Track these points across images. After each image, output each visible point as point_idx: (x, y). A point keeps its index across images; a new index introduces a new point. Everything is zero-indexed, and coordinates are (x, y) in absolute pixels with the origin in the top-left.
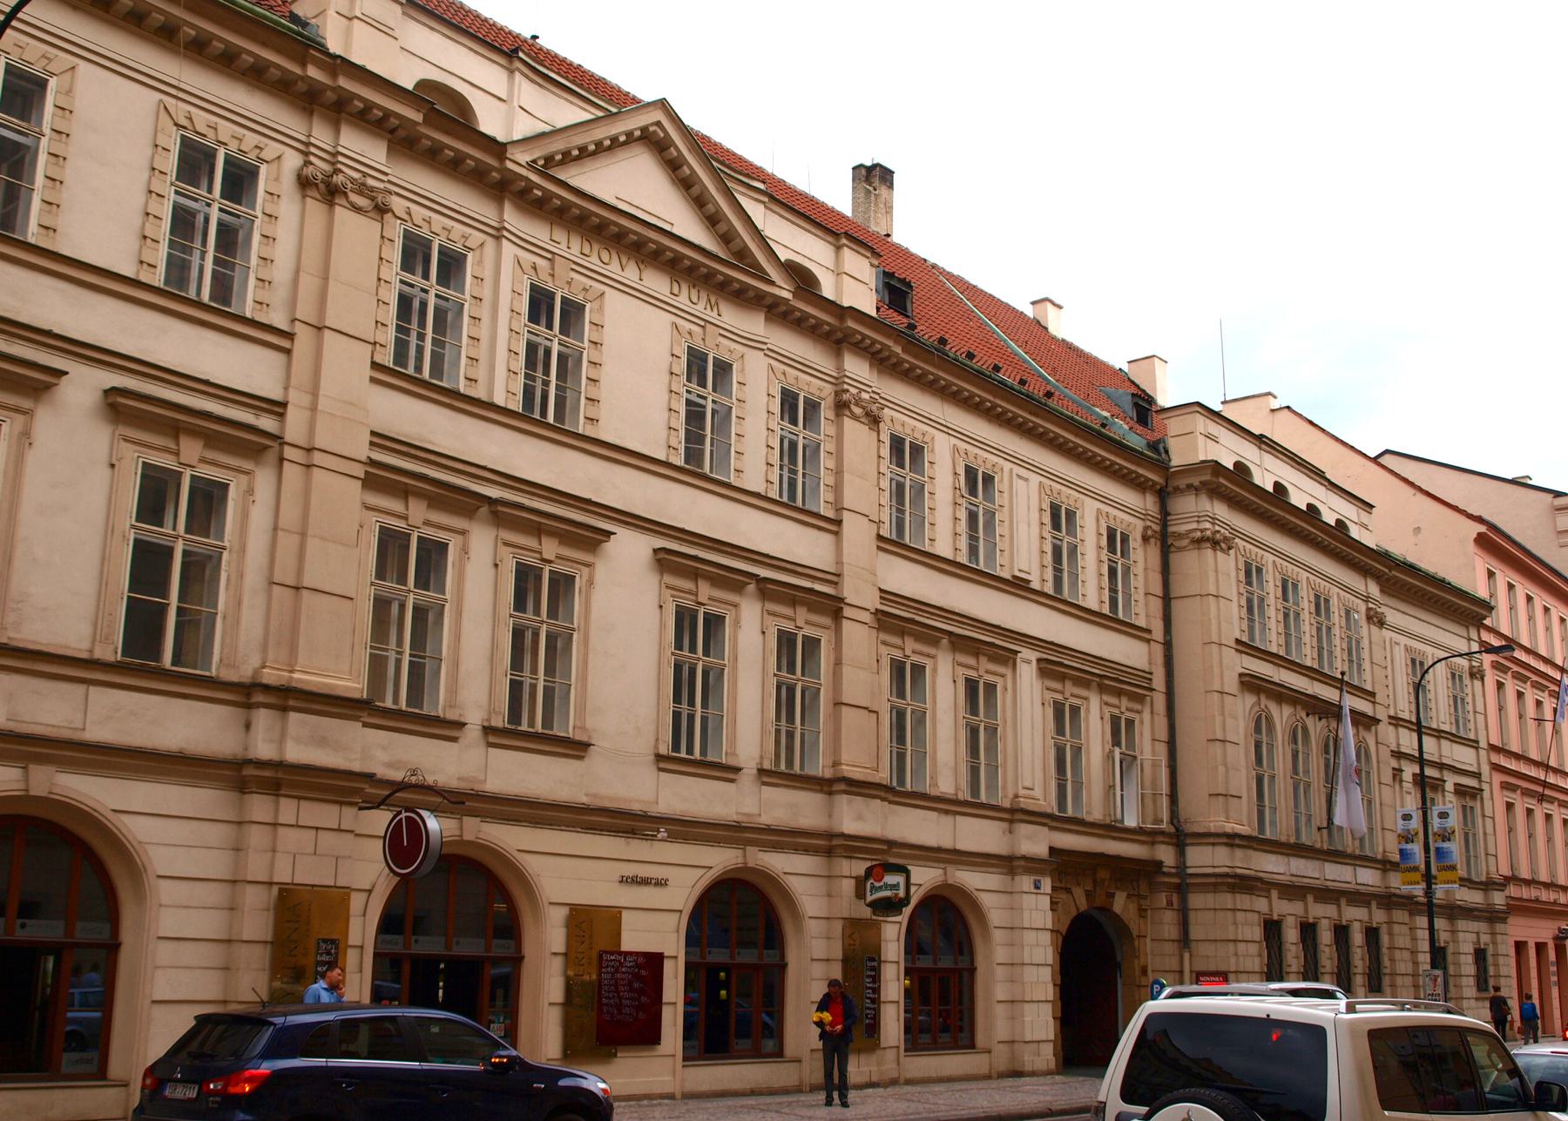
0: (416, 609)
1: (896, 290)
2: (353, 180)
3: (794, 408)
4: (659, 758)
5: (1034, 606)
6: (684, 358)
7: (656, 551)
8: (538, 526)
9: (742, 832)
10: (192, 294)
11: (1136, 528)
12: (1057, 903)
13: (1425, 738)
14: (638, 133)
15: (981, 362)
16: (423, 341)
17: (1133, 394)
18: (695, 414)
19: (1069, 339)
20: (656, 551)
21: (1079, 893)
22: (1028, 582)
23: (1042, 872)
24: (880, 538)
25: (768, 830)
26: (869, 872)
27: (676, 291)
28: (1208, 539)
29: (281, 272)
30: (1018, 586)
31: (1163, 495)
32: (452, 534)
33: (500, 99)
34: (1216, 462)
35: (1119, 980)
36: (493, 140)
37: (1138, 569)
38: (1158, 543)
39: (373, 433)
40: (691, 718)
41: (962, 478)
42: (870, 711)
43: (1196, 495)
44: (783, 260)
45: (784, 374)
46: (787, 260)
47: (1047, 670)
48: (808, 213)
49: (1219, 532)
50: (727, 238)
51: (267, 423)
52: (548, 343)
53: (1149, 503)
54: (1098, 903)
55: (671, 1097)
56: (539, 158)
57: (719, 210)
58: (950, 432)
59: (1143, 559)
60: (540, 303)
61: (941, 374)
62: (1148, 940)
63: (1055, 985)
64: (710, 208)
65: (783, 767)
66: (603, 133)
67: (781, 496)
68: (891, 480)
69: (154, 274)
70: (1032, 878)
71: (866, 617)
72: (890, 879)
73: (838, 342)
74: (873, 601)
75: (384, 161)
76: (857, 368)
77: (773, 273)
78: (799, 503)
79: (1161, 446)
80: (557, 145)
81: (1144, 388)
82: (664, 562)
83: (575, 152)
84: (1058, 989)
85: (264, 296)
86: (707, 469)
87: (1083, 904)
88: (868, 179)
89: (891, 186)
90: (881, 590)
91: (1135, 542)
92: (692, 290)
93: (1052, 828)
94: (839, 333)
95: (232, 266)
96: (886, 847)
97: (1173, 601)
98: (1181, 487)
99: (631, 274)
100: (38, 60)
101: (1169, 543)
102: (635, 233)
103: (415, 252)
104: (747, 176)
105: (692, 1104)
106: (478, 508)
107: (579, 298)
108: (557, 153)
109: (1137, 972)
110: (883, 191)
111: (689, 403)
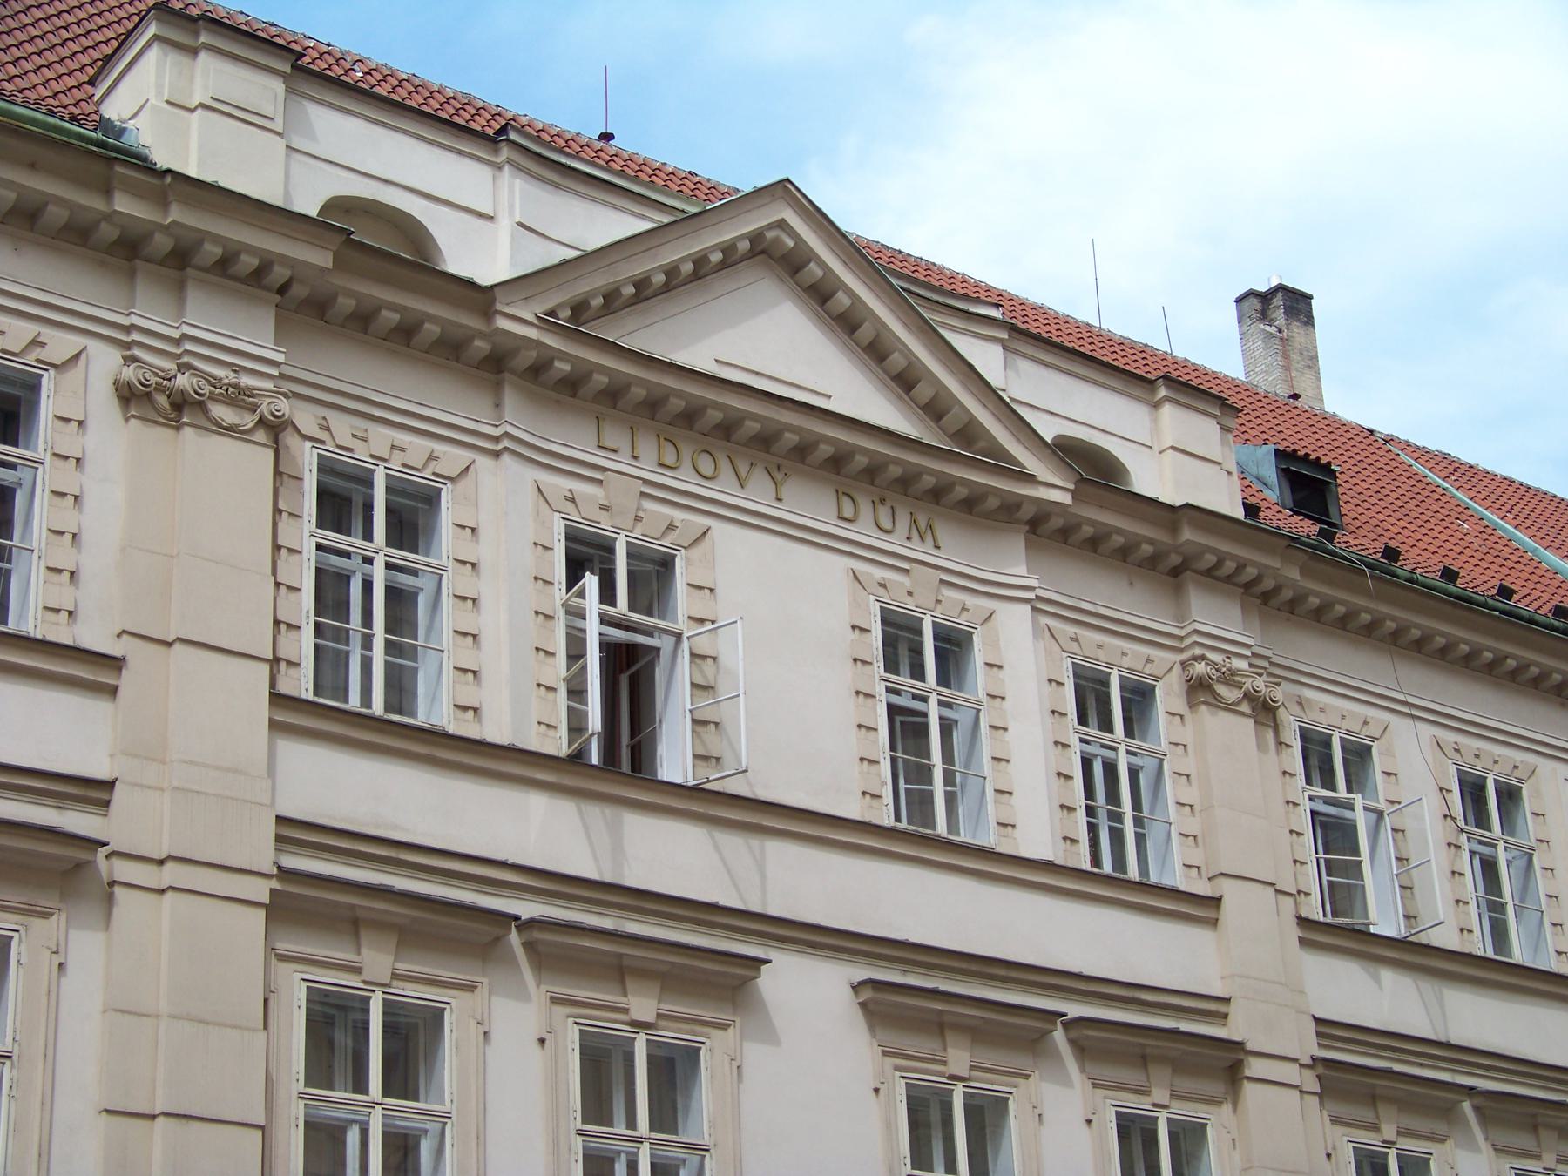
0: (388, 1136)
2: (215, 382)
3: (1328, 760)
7: (856, 988)
10: (354, 702)
15: (1527, 600)
20: (856, 988)
24: (1303, 922)
27: (848, 511)
29: (96, 560)
33: (481, 215)
36: (469, 284)
39: (280, 820)
41: (1456, 797)
44: (1049, 439)
45: (1076, 640)
46: (1057, 437)
50: (936, 410)
52: (1109, 754)
56: (560, 305)
57: (913, 362)
58: (1415, 712)
61: (1385, 609)
64: (897, 361)
66: (678, 252)
68: (1472, 853)
74: (1308, 1045)
75: (1022, 570)
78: (1133, 873)
80: (592, 284)
85: (468, 696)
86: (941, 828)
88: (1264, 316)
89: (1309, 321)
90: (1317, 1020)
95: (411, 653)
99: (758, 495)
100: (1362, 729)
104: (965, 297)
106: (497, 939)
110: (1297, 331)
111: (893, 710)
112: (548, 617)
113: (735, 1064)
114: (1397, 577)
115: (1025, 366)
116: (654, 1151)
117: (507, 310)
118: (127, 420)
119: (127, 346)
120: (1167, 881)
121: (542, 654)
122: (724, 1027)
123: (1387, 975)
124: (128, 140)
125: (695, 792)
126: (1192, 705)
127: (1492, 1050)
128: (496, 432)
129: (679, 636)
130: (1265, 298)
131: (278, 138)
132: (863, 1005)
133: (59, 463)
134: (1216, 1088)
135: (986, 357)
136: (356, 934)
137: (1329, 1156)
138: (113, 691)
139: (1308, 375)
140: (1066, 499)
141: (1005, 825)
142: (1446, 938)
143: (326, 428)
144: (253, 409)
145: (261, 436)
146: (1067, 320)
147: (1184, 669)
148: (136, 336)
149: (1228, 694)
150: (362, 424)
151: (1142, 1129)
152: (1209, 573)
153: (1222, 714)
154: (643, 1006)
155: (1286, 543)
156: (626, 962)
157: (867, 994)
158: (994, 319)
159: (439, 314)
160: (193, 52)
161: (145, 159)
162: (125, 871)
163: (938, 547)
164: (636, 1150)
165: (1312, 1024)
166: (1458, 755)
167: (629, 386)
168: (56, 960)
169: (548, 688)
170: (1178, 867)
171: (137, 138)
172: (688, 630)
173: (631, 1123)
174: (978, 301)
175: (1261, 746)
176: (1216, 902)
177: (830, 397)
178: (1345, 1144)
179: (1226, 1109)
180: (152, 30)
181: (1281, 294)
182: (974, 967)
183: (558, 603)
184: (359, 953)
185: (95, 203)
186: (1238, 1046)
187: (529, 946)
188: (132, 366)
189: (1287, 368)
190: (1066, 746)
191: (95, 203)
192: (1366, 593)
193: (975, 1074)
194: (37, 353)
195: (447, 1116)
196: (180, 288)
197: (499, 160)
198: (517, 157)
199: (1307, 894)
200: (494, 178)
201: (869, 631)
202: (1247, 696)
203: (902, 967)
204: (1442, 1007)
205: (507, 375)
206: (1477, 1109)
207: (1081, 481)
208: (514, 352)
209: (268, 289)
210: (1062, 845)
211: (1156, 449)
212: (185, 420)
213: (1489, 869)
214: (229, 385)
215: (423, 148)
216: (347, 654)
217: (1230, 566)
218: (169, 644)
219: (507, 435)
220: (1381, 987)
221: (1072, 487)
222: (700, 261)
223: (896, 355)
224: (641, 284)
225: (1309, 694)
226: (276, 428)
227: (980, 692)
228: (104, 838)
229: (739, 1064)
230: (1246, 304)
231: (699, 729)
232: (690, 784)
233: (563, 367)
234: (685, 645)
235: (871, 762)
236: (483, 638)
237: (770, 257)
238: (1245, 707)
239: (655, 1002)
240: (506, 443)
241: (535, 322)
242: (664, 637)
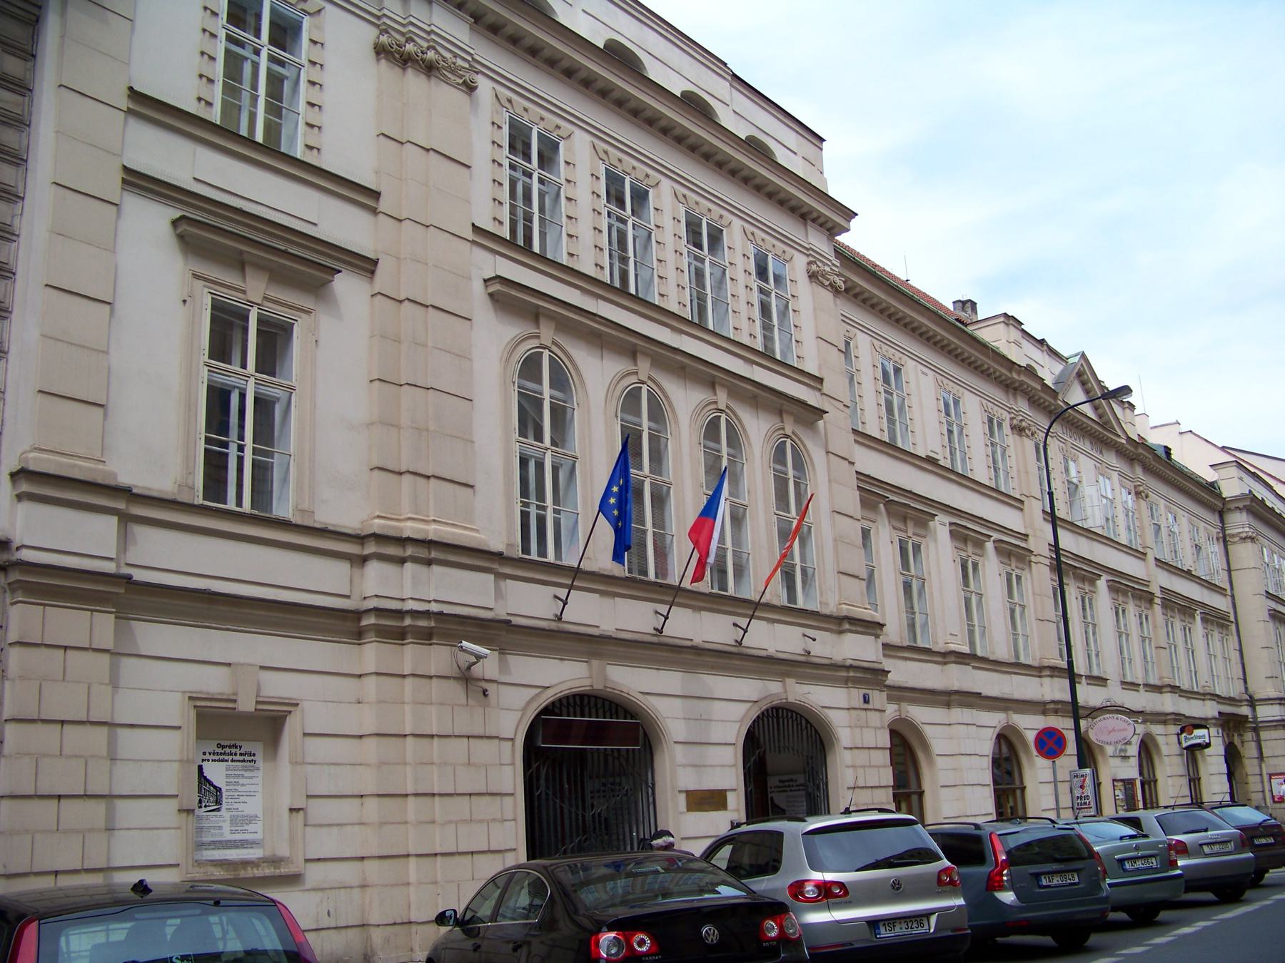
0: (257, 400)
4: (1123, 683)
5: (1111, 549)
7: (175, 223)
9: (836, 671)
13: (1060, 531)
20: (175, 223)
25: (1152, 714)
26: (1182, 730)
31: (1221, 514)
40: (541, 521)
45: (753, 234)
47: (1114, 588)
53: (1215, 519)
70: (862, 692)
72: (1197, 732)
73: (1015, 389)
90: (1161, 587)
127: (162, 178)
136: (1083, 581)
140: (1124, 441)
150: (901, 355)
164: (245, 383)
173: (244, 366)
186: (1153, 594)
213: (699, 275)
227: (304, 56)
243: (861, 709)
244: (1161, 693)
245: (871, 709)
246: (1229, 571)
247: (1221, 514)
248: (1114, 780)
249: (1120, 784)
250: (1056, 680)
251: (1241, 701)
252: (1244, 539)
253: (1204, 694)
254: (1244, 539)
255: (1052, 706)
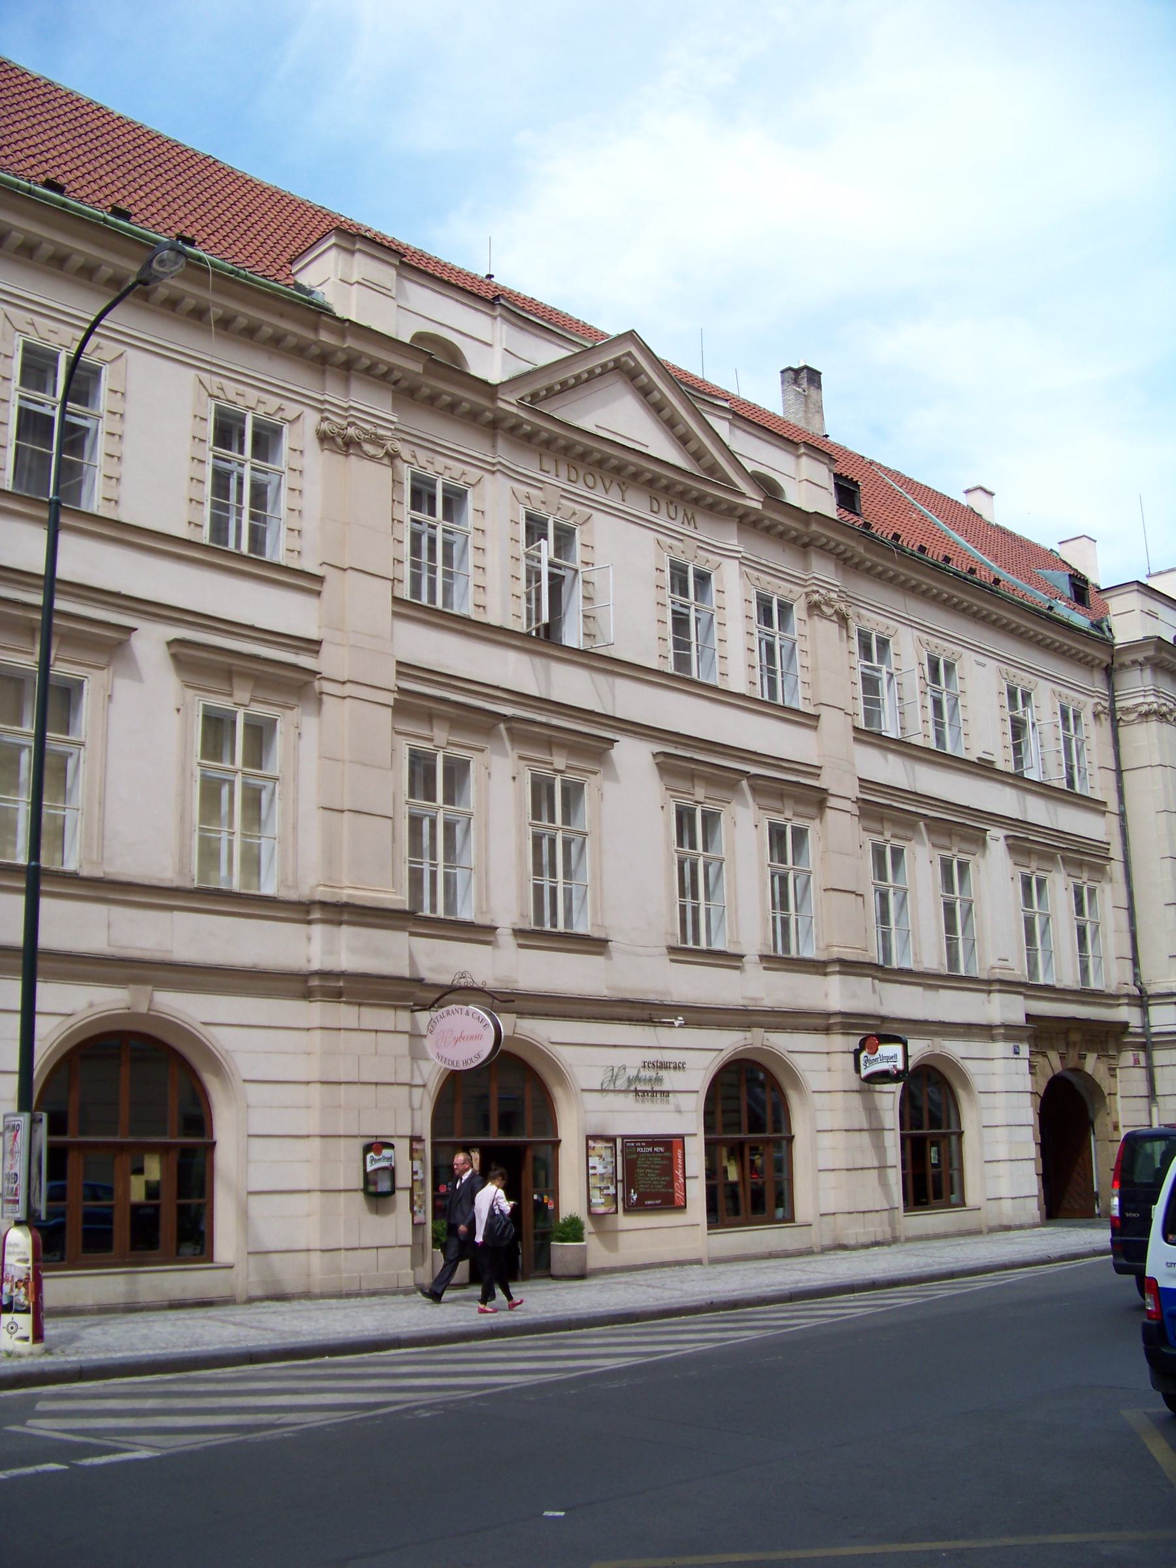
1: (847, 492)
2: (366, 432)
4: (672, 950)
6: (668, 570)
7: (655, 755)
8: (549, 740)
10: (231, 546)
11: (1088, 706)
12: (1035, 1066)
14: (611, 365)
16: (435, 573)
17: (1070, 575)
18: (680, 622)
19: (1002, 524)
20: (655, 755)
21: (1054, 1056)
22: (992, 762)
23: (1020, 1040)
24: (856, 729)
26: (862, 1046)
28: (1155, 712)
29: (310, 523)
30: (983, 768)
31: (1109, 672)
32: (473, 752)
34: (1159, 637)
35: (1092, 1137)
36: (486, 383)
37: (1092, 743)
38: (1109, 719)
39: (399, 663)
41: (926, 667)
42: (857, 895)
43: (1141, 670)
44: (749, 471)
46: (753, 472)
48: (746, 415)
49: (1165, 704)
50: (697, 456)
51: (304, 661)
52: (770, 639)
53: (1098, 684)
54: (1071, 1065)
55: (699, 1262)
57: (689, 430)
59: (1095, 735)
60: (535, 528)
61: (901, 570)
62: (1118, 1097)
63: (1036, 1144)
64: (681, 429)
65: (780, 952)
67: (763, 696)
69: (202, 533)
71: (854, 809)
72: (886, 1050)
74: (855, 792)
75: (735, 542)
76: (823, 571)
77: (743, 486)
78: (780, 701)
79: (1104, 625)
80: (540, 384)
81: (1076, 568)
82: (667, 766)
83: (558, 387)
84: (1038, 1147)
85: (296, 544)
86: (694, 675)
87: (1057, 1066)
88: (796, 382)
89: (819, 387)
90: (860, 779)
91: (1087, 717)
92: (670, 506)
93: (1027, 997)
94: (805, 537)
95: (264, 519)
96: (879, 1023)
97: (1124, 773)
98: (1126, 663)
99: (613, 499)
101: (1118, 718)
102: (616, 457)
103: (422, 495)
104: (709, 395)
105: (720, 1268)
106: (494, 726)
107: (570, 523)
108: (541, 389)
109: (1110, 1128)
110: (813, 391)
112: (518, 560)
113: (600, 792)
114: (906, 552)
115: (738, 433)
116: (447, 817)
117: (503, 397)
118: (322, 450)
119: (322, 411)
120: (794, 706)
121: (514, 579)
122: (595, 773)
123: (891, 757)
124: (318, 298)
125: (584, 653)
126: (810, 615)
128: (494, 461)
129: (576, 571)
130: (797, 372)
131: (392, 300)
132: (657, 764)
133: (292, 473)
134: (812, 811)
135: (721, 427)
136: (431, 723)
137: (861, 846)
138: (318, 594)
139: (817, 417)
140: (759, 506)
141: (723, 674)
142: (918, 740)
143: (415, 457)
144: (383, 446)
145: (386, 461)
146: (764, 411)
147: (807, 597)
148: (327, 406)
149: (828, 611)
150: (431, 454)
151: (688, 813)
152: (821, 547)
153: (825, 621)
154: (560, 762)
155: (860, 534)
156: (696, 772)
157: (661, 759)
158: (726, 408)
159: (470, 398)
160: (352, 252)
161: (330, 311)
162: (328, 687)
163: (696, 528)
165: (857, 780)
166: (757, 581)
167: (286, 336)
168: (297, 731)
169: (517, 597)
170: (471, 606)
171: (323, 298)
172: (582, 569)
174: (716, 397)
175: (841, 639)
176: (817, 717)
177: (648, 446)
178: (868, 840)
179: (817, 821)
180: (333, 240)
181: (805, 371)
182: (708, 746)
183: (522, 553)
184: (432, 731)
185: (311, 336)
186: (825, 790)
187: (508, 730)
188: (326, 422)
189: (806, 412)
190: (752, 634)
191: (311, 336)
192: (893, 561)
193: (707, 800)
194: (281, 414)
195: (810, 872)
196: (347, 381)
197: (495, 314)
198: (505, 313)
199: (857, 715)
200: (493, 324)
201: (664, 571)
202: (836, 612)
203: (675, 745)
204: (914, 774)
205: (499, 431)
206: (926, 825)
207: (767, 497)
208: (504, 419)
209: (388, 382)
210: (749, 686)
211: (798, 480)
212: (351, 452)
213: (937, 704)
214: (372, 434)
215: (459, 306)
216: (228, 518)
217: (832, 544)
218: (345, 570)
219: (500, 463)
220: (888, 763)
221: (762, 500)
222: (591, 372)
223: (681, 426)
224: (563, 384)
225: (863, 611)
226: (393, 456)
228: (320, 671)
229: (109, 693)
230: (786, 374)
231: (586, 620)
232: (582, 649)
233: (527, 428)
234: (580, 576)
235: (663, 639)
236: (487, 569)
237: (622, 371)
238: (835, 618)
239: (447, 734)
240: (499, 467)
241: (516, 404)
242: (567, 570)
243: (1012, 1058)
244: (825, 974)
245: (1021, 1059)
246: (1119, 772)
247: (1109, 672)
248: (589, 1138)
249: (599, 1145)
250: (345, 930)
251: (1117, 997)
252: (1146, 715)
253: (989, 982)
254: (1146, 715)
255: (838, 1019)
